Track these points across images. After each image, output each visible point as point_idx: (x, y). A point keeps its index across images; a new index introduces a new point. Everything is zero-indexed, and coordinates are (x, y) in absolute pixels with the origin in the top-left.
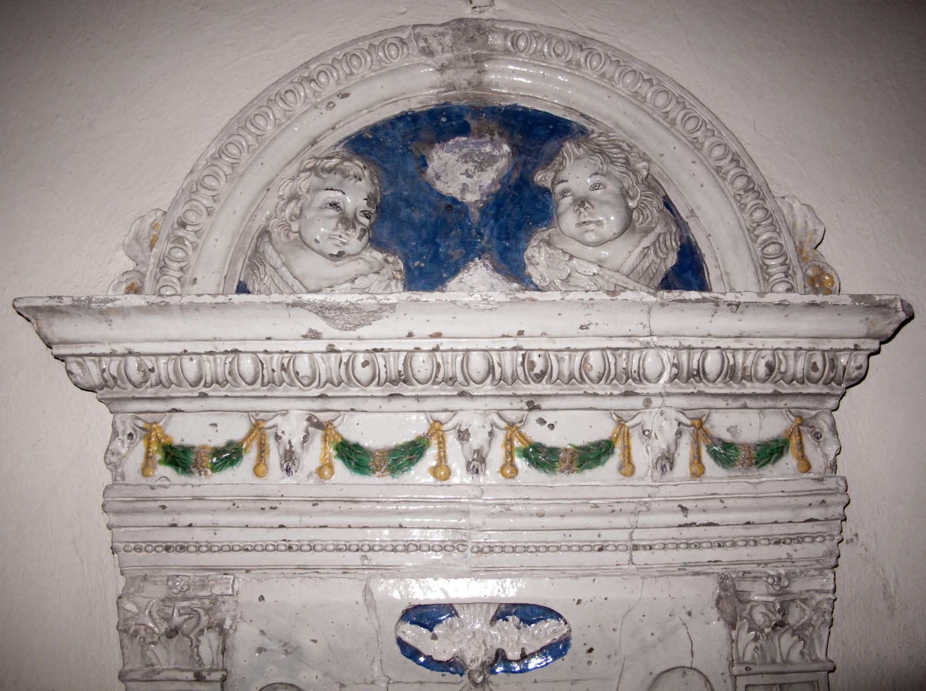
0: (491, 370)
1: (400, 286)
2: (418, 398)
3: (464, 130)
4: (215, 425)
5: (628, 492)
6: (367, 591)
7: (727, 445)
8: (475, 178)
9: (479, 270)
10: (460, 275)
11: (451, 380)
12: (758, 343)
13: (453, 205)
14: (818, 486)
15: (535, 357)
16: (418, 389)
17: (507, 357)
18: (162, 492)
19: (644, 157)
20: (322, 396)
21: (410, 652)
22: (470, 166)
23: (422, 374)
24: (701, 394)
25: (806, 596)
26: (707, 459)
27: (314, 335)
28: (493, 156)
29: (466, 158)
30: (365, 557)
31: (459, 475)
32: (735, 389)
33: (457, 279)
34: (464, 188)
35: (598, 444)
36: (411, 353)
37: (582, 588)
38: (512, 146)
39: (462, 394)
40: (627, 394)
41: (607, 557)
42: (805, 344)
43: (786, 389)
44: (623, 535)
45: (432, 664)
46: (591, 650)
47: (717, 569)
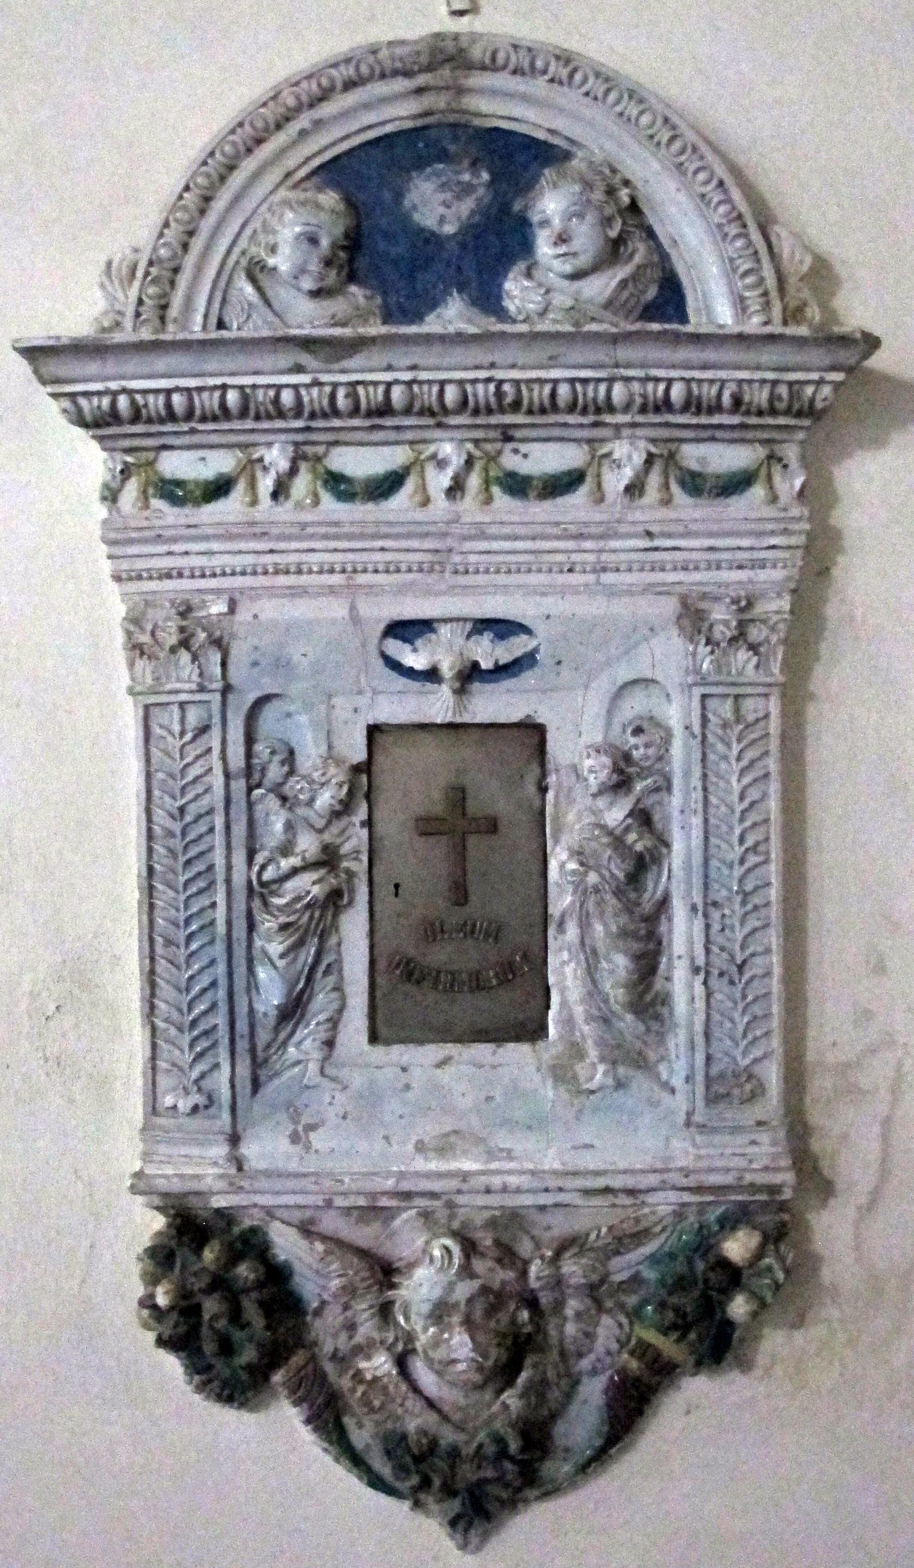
0: (464, 402)
1: (379, 321)
2: (398, 428)
3: (444, 156)
4: (203, 459)
5: (598, 517)
6: (353, 608)
7: (694, 475)
8: (454, 209)
9: (457, 305)
10: (439, 310)
11: (427, 411)
12: (723, 374)
13: (430, 239)
14: (782, 515)
15: (506, 387)
16: (395, 421)
17: (480, 388)
18: (158, 523)
19: (627, 183)
20: (308, 429)
21: (395, 665)
22: (448, 196)
23: (782, 406)
24: (667, 425)
25: (764, 616)
26: (675, 488)
27: (299, 369)
28: (472, 185)
29: (443, 187)
30: (349, 578)
31: (440, 502)
32: (704, 420)
33: (435, 313)
34: (442, 220)
35: (569, 473)
36: (389, 385)
37: (552, 605)
38: (492, 173)
39: (439, 425)
40: (596, 425)
41: (576, 579)
42: (770, 376)
43: (754, 420)
44: (591, 558)
45: (410, 673)
46: (559, 663)
47: (678, 589)
